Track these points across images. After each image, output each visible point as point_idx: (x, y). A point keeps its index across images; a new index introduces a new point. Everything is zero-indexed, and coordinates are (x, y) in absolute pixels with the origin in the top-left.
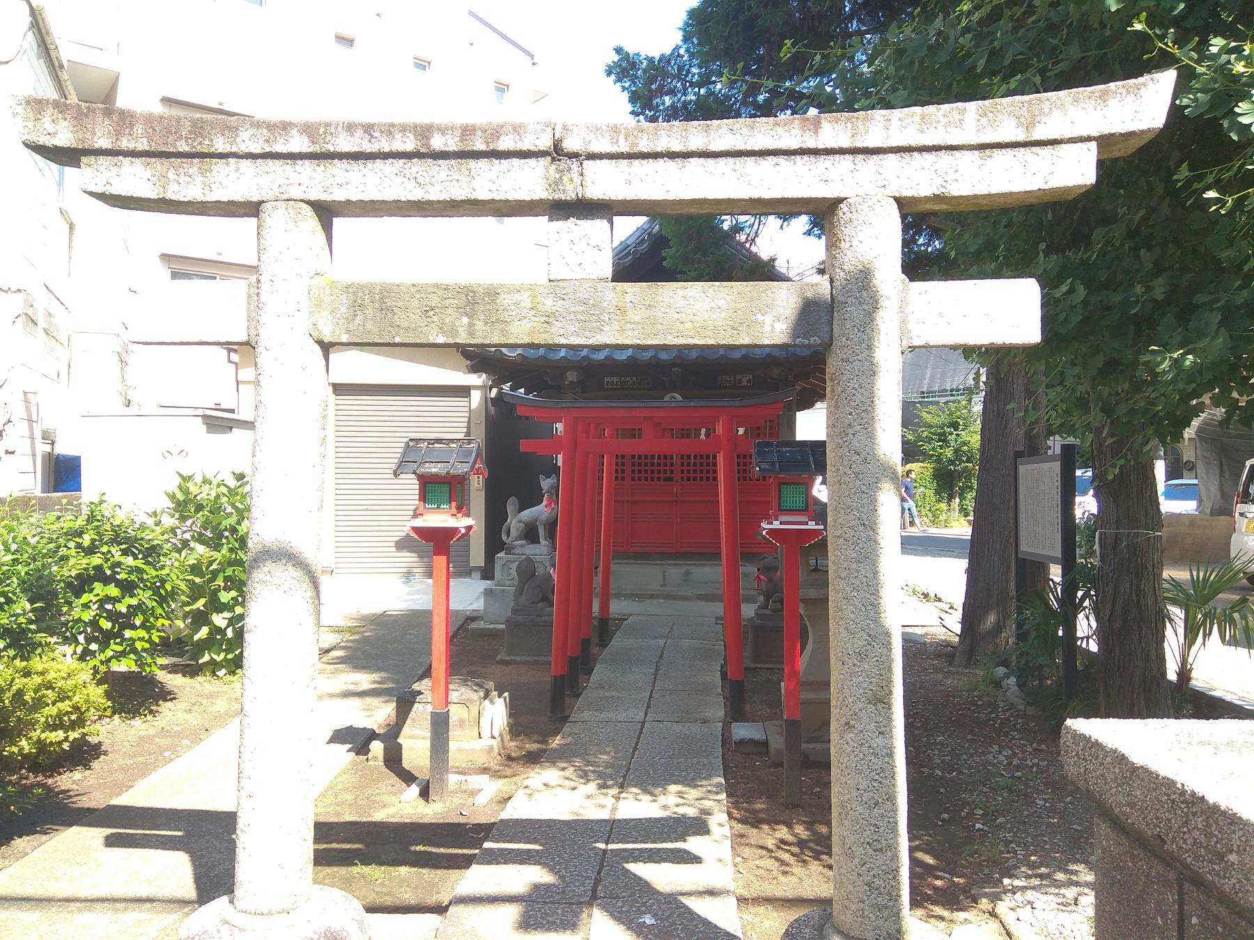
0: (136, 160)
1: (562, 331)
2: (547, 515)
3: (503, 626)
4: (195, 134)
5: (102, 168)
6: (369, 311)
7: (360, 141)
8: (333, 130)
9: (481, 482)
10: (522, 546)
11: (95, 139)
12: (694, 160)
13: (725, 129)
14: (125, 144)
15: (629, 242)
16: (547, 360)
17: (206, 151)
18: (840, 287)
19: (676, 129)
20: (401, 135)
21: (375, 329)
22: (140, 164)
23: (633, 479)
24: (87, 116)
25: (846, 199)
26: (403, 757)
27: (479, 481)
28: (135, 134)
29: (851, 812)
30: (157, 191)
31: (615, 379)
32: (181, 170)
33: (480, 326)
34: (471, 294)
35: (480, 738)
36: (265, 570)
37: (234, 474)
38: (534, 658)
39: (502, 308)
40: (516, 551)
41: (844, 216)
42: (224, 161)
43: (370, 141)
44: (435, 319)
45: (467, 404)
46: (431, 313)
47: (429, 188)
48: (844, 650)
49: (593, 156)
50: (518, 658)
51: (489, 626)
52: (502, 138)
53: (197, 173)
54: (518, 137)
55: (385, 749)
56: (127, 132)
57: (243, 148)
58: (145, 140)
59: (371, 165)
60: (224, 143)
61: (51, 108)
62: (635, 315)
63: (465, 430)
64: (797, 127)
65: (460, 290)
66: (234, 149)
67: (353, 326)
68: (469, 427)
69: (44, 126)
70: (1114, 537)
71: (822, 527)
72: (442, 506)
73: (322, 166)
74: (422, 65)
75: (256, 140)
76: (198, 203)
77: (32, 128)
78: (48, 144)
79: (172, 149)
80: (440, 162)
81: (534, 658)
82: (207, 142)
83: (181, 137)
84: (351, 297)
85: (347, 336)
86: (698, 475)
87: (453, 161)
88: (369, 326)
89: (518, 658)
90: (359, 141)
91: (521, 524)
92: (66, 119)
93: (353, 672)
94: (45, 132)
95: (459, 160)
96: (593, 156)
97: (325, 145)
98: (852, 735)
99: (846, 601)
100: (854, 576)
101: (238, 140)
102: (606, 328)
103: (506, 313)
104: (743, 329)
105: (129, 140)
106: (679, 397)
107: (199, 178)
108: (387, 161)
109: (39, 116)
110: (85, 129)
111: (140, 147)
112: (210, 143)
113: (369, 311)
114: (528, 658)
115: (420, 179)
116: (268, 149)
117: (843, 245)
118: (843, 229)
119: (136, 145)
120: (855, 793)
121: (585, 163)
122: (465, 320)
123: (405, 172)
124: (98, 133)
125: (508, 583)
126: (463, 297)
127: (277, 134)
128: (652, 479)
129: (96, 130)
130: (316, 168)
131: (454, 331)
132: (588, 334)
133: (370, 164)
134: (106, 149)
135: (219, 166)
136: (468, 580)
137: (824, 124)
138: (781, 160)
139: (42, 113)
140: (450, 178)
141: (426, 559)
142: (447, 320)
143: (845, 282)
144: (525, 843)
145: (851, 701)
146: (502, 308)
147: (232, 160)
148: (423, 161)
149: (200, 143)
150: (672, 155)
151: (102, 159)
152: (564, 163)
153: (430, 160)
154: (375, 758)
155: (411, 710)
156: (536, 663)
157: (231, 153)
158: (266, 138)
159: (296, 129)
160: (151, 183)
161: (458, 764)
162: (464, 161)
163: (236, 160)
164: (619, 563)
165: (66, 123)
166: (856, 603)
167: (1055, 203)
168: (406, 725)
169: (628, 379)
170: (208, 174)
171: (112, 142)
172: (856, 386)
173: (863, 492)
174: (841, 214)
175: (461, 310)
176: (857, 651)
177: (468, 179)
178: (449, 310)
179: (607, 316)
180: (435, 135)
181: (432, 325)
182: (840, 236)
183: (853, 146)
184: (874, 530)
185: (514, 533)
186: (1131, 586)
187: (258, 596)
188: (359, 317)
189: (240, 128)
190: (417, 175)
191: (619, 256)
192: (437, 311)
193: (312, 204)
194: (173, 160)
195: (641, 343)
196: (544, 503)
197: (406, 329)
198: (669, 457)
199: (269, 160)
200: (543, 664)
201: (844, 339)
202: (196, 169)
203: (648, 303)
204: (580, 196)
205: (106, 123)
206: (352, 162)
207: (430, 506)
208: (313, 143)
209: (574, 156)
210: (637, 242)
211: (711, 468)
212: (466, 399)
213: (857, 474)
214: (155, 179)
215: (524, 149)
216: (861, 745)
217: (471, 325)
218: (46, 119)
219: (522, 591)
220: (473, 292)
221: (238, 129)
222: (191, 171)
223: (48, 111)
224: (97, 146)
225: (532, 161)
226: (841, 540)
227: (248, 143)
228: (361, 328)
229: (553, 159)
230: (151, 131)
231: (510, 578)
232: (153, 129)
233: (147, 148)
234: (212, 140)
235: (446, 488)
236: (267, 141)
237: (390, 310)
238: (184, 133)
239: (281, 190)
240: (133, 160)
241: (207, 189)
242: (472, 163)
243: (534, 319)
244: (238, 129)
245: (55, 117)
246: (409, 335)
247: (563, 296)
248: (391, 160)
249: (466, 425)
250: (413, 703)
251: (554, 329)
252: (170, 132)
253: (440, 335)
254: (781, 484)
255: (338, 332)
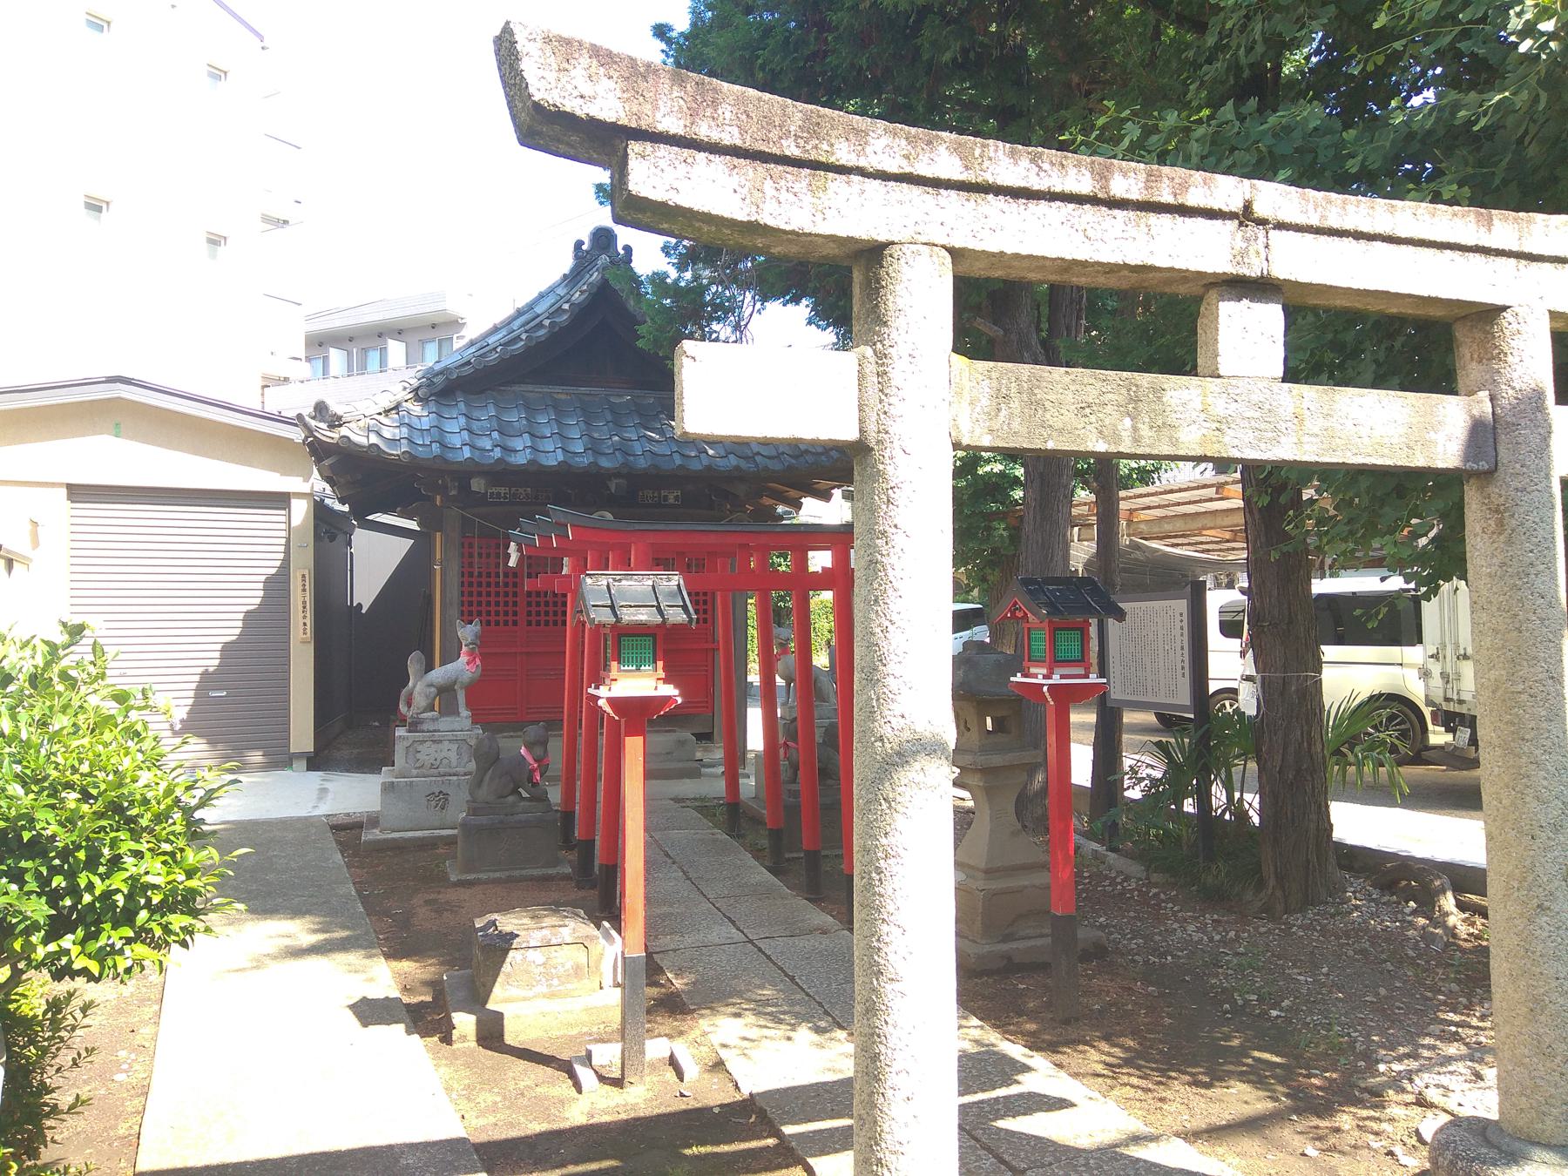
0: (716, 158)
1: (1236, 442)
2: (470, 675)
3: (455, 832)
4: (809, 132)
5: (663, 164)
6: (1015, 405)
7: (1026, 173)
8: (992, 154)
9: (308, 631)
10: (434, 720)
11: (658, 116)
12: (1378, 244)
13: (1409, 212)
14: (704, 131)
15: (539, 309)
16: (446, 461)
17: (824, 160)
18: (1508, 407)
19: (1362, 205)
20: (1075, 170)
21: (1024, 430)
22: (721, 167)
23: (530, 624)
24: (645, 78)
25: (1509, 307)
26: (506, 1030)
27: (305, 630)
28: (721, 118)
29: (1550, 1005)
30: (747, 210)
31: (503, 490)
32: (783, 183)
33: (1145, 431)
34: (1134, 389)
35: (601, 988)
36: (917, 766)
37: (64, 625)
38: (507, 873)
39: (1169, 409)
40: (425, 727)
41: (1510, 327)
42: (844, 177)
43: (1038, 175)
44: (1093, 418)
45: (283, 519)
46: (1088, 411)
47: (1098, 244)
48: (1534, 822)
49: (1281, 226)
50: (483, 876)
51: (390, 836)
52: (1192, 189)
53: (805, 190)
54: (1208, 192)
55: (479, 1022)
56: (708, 114)
57: (871, 162)
58: (735, 131)
59: (1034, 206)
60: (849, 152)
61: (587, 56)
62: (1314, 425)
63: (281, 556)
64: (1473, 220)
65: (1121, 383)
66: (862, 163)
67: (996, 425)
68: (287, 552)
69: (574, 82)
70: (1281, 682)
71: (1104, 680)
72: (643, 667)
73: (972, 201)
74: (98, 24)
75: (892, 154)
76: (805, 234)
77: (553, 82)
78: (578, 113)
79: (775, 150)
80: (1116, 212)
81: (507, 873)
82: (825, 146)
83: (787, 134)
84: (995, 384)
85: (990, 437)
86: (543, 618)
87: (1131, 213)
88: (1016, 425)
89: (483, 876)
90: (1025, 173)
91: (433, 689)
92: (611, 78)
93: (252, 920)
94: (576, 93)
95: (1138, 213)
96: (1281, 226)
97: (982, 173)
98: (1545, 919)
99: (1534, 767)
100: (1545, 736)
101: (869, 150)
102: (1283, 439)
103: (1174, 415)
104: (1418, 448)
105: (710, 127)
106: (609, 516)
107: (808, 199)
108: (1052, 204)
109: (566, 66)
110: (641, 99)
111: (727, 141)
112: (829, 149)
113: (1015, 405)
114: (497, 875)
115: (1090, 233)
116: (908, 170)
117: (1510, 359)
118: (1510, 341)
119: (723, 136)
120: (1554, 984)
121: (1272, 233)
122: (1128, 422)
123: (1073, 221)
124: (662, 108)
125: (415, 772)
126: (1124, 391)
127: (919, 149)
128: (547, 623)
129: (660, 102)
130: (966, 203)
131: (1117, 438)
132: (1263, 446)
133: (1032, 205)
134: (674, 136)
135: (837, 182)
136: (288, 772)
137: (1496, 221)
138: (1456, 255)
139: (572, 61)
140: (1125, 235)
141: (220, 746)
142: (1107, 422)
143: (1515, 401)
144: (832, 1118)
145: (1545, 880)
146: (1169, 409)
147: (855, 178)
148: (1097, 208)
149: (816, 147)
150: (1358, 235)
151: (663, 150)
152: (1252, 229)
153: (1104, 209)
154: (464, 1038)
155: (503, 962)
156: (510, 880)
157: (857, 167)
158: (905, 152)
159: (945, 146)
160: (738, 197)
161: (585, 1029)
162: (1144, 213)
163: (860, 178)
164: (512, 737)
165: (611, 84)
166: (1549, 767)
167: (1402, 318)
168: (497, 984)
169: (521, 490)
170: (821, 195)
171: (686, 126)
172: (1537, 520)
173: (1550, 641)
174: (1506, 324)
175: (1121, 409)
176: (1552, 821)
177: (1147, 238)
178: (1109, 406)
179: (1284, 425)
180: (1116, 175)
181: (1088, 427)
182: (1506, 349)
183: (1521, 250)
184: (1560, 683)
185: (420, 701)
186: (1302, 733)
187: (908, 804)
188: (1003, 413)
189: (871, 133)
190: (1088, 227)
191: (527, 327)
192: (1095, 408)
193: (952, 251)
194: (772, 166)
195: (1319, 460)
196: (463, 659)
197: (1061, 431)
198: (542, 595)
199: (904, 185)
200: (520, 881)
201: (1518, 466)
202: (804, 184)
203: (1325, 412)
204: (1265, 272)
205: (675, 94)
206: (1011, 200)
207: (626, 668)
208: (967, 168)
209: (1262, 222)
210: (551, 311)
211: (559, 609)
212: (283, 512)
213: (1542, 620)
214: (745, 191)
215: (1216, 207)
216: (1558, 928)
217: (1135, 429)
218: (578, 74)
219: (482, 781)
220: (1137, 386)
221: (868, 135)
222: (797, 186)
223: (581, 60)
224: (661, 128)
225: (1218, 223)
226: (1524, 697)
227: (880, 156)
228: (1005, 428)
229: (1241, 224)
230: (744, 117)
231: (417, 765)
232: (748, 116)
233: (739, 143)
234: (832, 145)
235: (648, 642)
236: (907, 157)
237: (1041, 404)
238: (792, 128)
239: (919, 229)
240: (712, 157)
241: (819, 216)
242: (1153, 218)
243: (1205, 424)
244: (868, 135)
245: (593, 70)
246: (1064, 439)
247: (1235, 397)
248: (1058, 203)
249: (282, 549)
250: (506, 952)
251: (1227, 439)
252: (771, 123)
253: (1100, 441)
254: (1056, 629)
255: (978, 431)
